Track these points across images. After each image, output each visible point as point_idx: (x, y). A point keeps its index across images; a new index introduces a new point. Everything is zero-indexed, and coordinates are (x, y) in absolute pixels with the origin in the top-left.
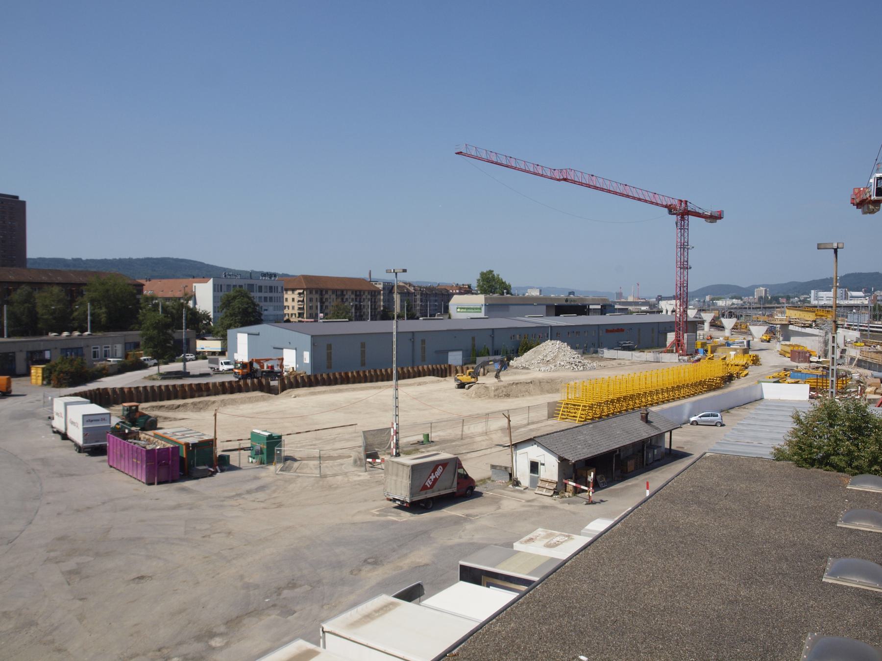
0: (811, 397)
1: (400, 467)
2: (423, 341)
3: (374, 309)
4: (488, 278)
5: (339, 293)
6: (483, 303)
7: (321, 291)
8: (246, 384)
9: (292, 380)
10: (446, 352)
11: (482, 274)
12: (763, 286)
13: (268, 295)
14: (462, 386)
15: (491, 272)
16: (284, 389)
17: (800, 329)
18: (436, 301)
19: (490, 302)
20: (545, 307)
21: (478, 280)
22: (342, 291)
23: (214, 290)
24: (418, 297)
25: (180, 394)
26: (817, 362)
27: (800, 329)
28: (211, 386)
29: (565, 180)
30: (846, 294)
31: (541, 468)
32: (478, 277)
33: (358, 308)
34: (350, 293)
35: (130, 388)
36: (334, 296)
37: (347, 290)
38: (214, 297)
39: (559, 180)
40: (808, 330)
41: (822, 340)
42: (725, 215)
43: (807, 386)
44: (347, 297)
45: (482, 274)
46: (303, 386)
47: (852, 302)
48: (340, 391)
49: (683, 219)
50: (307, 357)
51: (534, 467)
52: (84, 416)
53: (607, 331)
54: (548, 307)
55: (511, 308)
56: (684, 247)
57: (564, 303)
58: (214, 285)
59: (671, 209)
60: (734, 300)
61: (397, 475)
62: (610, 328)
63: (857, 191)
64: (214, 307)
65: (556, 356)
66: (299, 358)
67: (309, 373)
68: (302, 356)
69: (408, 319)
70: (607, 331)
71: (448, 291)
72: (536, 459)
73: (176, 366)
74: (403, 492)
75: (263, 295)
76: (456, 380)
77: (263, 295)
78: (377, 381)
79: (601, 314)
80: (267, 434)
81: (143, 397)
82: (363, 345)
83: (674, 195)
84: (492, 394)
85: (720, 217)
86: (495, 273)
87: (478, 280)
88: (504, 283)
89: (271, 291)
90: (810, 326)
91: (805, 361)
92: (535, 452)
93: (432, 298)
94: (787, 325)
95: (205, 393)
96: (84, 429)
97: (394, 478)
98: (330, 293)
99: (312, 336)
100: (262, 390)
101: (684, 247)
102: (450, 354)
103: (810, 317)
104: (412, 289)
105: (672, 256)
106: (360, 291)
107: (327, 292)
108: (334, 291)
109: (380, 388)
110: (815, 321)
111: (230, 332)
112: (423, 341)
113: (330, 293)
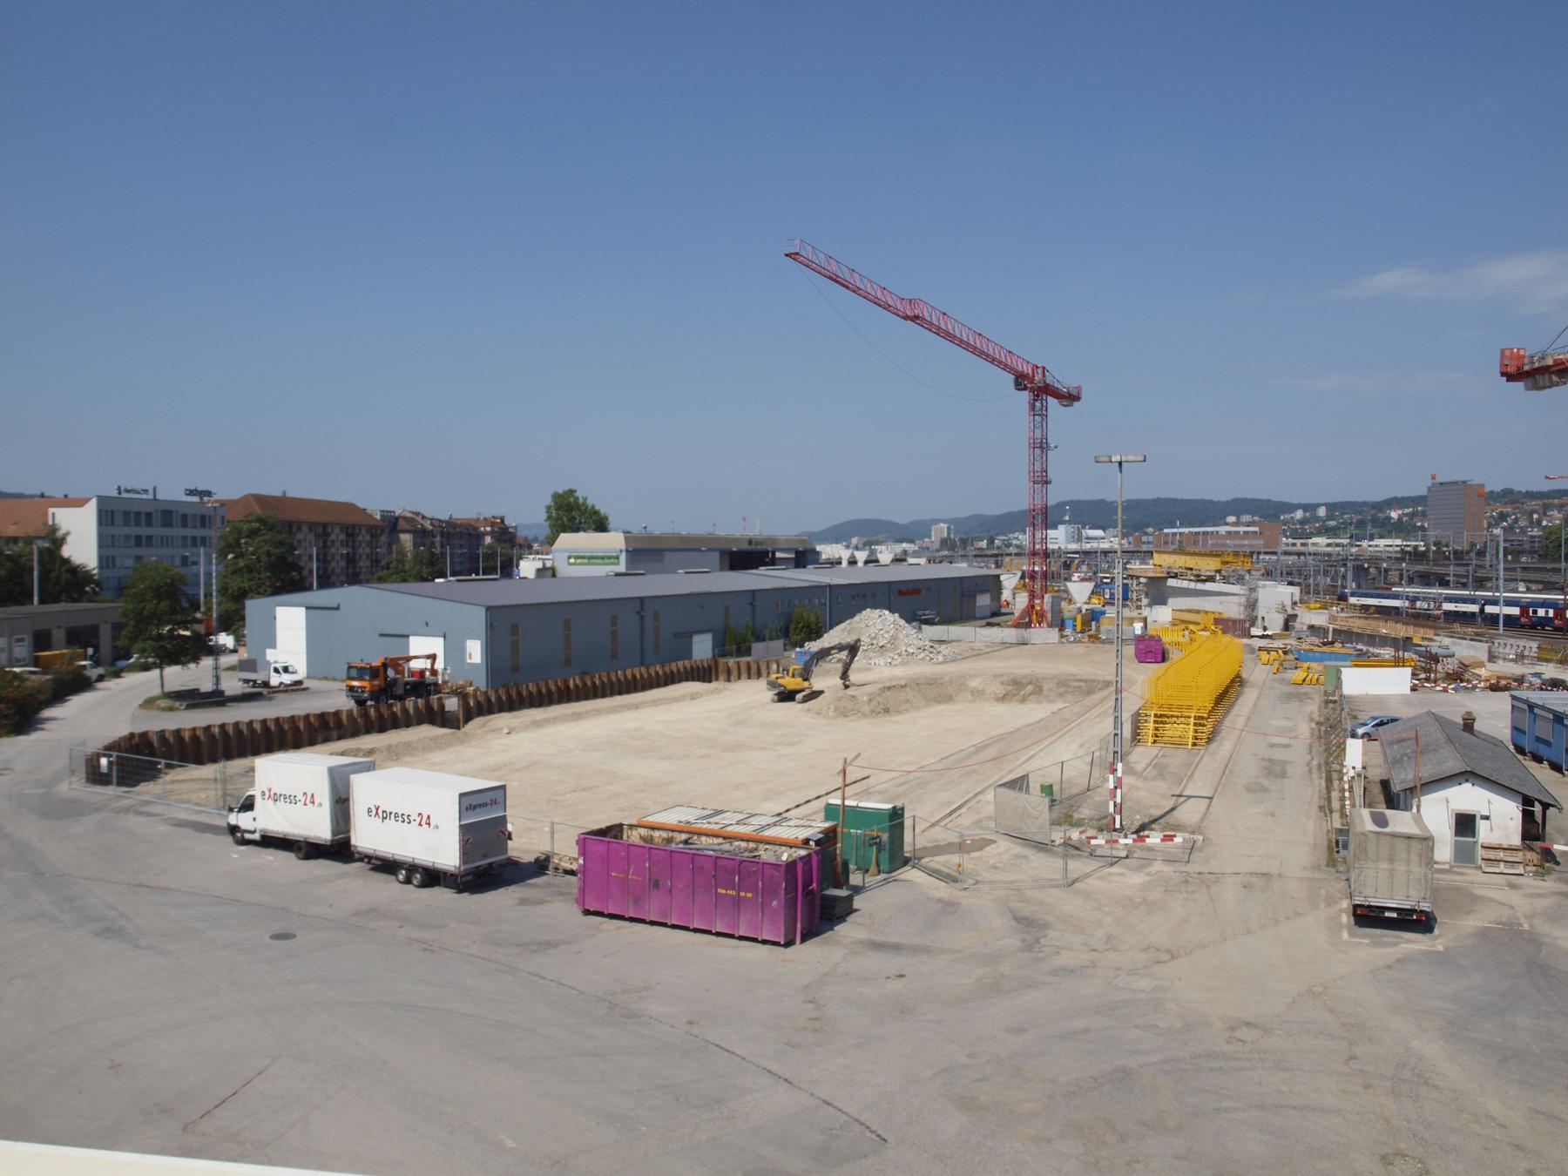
0: (1414, 689)
1: (1401, 845)
2: (656, 616)
3: (324, 560)
4: (568, 504)
5: (320, 530)
6: (623, 546)
7: (290, 526)
9: (481, 699)
10: (689, 635)
11: (556, 497)
12: (944, 521)
14: (786, 696)
15: (572, 492)
17: (1192, 585)
18: (461, 546)
21: (548, 508)
22: (325, 526)
23: (101, 522)
24: (438, 539)
25: (289, 736)
26: (1263, 637)
27: (1192, 585)
28: (344, 717)
29: (915, 318)
30: (1080, 534)
31: (1482, 826)
32: (549, 501)
33: (351, 560)
35: (194, 729)
36: (311, 537)
37: (333, 525)
39: (906, 318)
40: (1209, 586)
41: (1243, 600)
42: (1083, 395)
43: (1409, 671)
44: (333, 537)
45: (556, 497)
46: (501, 710)
47: (1087, 547)
48: (578, 717)
49: (1037, 397)
50: (475, 651)
51: (1465, 824)
53: (901, 593)
54: (723, 553)
55: (668, 555)
57: (746, 547)
59: (1021, 381)
60: (905, 545)
61: (1391, 860)
63: (1507, 353)
64: (101, 558)
65: (894, 638)
70: (901, 593)
71: (476, 529)
72: (1467, 807)
73: (197, 676)
74: (1412, 893)
75: (189, 532)
76: (773, 685)
78: (612, 694)
79: (797, 566)
80: (890, 806)
81: (220, 748)
82: (568, 625)
83: (1031, 352)
86: (580, 494)
87: (548, 508)
88: (596, 513)
89: (203, 525)
90: (1211, 579)
93: (457, 542)
95: (335, 733)
97: (1385, 865)
98: (305, 529)
99: (489, 609)
100: (432, 722)
103: (1208, 565)
106: (354, 526)
107: (299, 529)
108: (312, 526)
109: (637, 707)
110: (1219, 571)
112: (656, 616)
113: (305, 529)
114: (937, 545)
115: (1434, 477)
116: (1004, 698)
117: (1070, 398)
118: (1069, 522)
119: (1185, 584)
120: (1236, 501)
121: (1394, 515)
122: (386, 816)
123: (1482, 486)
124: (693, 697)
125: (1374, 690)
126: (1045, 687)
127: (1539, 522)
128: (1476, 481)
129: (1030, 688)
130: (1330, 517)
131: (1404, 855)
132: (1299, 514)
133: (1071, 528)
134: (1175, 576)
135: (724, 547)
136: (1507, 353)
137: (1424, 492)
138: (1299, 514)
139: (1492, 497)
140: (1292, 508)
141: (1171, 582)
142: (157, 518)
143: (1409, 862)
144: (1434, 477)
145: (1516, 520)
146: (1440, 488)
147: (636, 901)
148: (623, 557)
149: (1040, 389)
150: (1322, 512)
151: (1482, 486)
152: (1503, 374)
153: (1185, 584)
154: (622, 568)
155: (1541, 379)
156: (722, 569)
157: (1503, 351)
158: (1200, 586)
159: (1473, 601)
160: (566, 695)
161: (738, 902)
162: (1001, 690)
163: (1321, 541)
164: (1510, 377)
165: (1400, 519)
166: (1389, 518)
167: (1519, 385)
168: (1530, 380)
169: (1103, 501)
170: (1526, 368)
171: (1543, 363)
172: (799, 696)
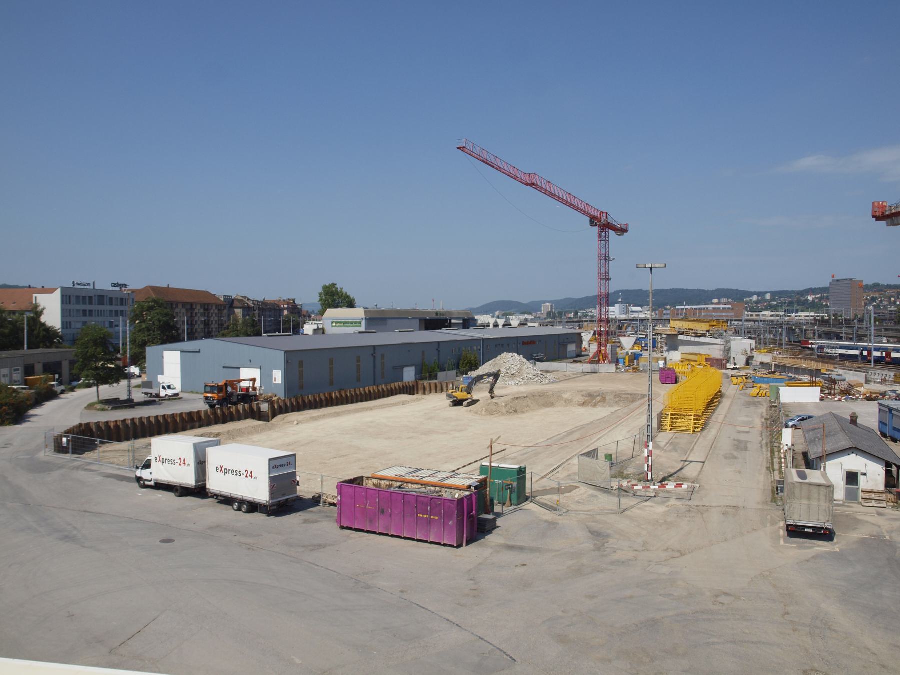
1: (815, 490)
4: (332, 292)
5: (189, 307)
6: (364, 317)
8: (238, 411)
11: (325, 288)
12: (549, 302)
13: (120, 308)
14: (458, 403)
15: (334, 285)
16: (274, 415)
17: (693, 339)
20: (418, 321)
21: (321, 294)
22: (192, 304)
23: (63, 302)
24: (257, 312)
25: (180, 426)
26: (734, 369)
27: (693, 339)
30: (627, 309)
31: (862, 479)
32: (321, 290)
33: (207, 324)
35: (116, 422)
37: (196, 304)
38: (63, 310)
39: (527, 184)
40: (703, 340)
41: (723, 347)
42: (630, 229)
43: (819, 389)
44: (197, 311)
48: (338, 415)
49: (603, 230)
50: (278, 377)
51: (852, 478)
52: (270, 460)
53: (524, 344)
57: (434, 317)
58: (63, 296)
60: (526, 316)
61: (809, 499)
62: (526, 341)
64: (63, 323)
65: (520, 369)
66: (266, 377)
68: (271, 376)
70: (524, 344)
71: (279, 306)
72: (853, 468)
74: (821, 518)
75: (114, 308)
76: (450, 396)
77: (114, 308)
79: (464, 328)
82: (331, 362)
83: (599, 204)
84: (504, 410)
85: (627, 231)
87: (321, 294)
88: (348, 297)
89: (122, 304)
90: (704, 336)
91: (723, 369)
93: (268, 313)
94: (677, 335)
95: (197, 424)
96: (272, 479)
97: (805, 502)
98: (180, 306)
99: (286, 352)
102: (405, 369)
103: (702, 328)
104: (251, 304)
105: (594, 265)
106: (208, 305)
107: (177, 306)
108: (184, 305)
110: (708, 331)
113: (180, 306)
115: (833, 277)
116: (583, 404)
117: (622, 231)
118: (621, 303)
119: (689, 338)
120: (718, 290)
121: (810, 298)
122: (227, 472)
124: (404, 403)
125: (798, 400)
128: (858, 279)
129: (599, 399)
130: (773, 300)
131: (816, 495)
132: (755, 298)
133: (623, 306)
136: (876, 205)
137: (828, 285)
138: (755, 298)
139: (867, 288)
140: (751, 294)
141: (681, 337)
142: (95, 300)
143: (819, 500)
144: (833, 277)
145: (881, 302)
147: (371, 521)
148: (363, 323)
149: (604, 226)
150: (768, 297)
152: (874, 217)
153: (689, 338)
154: (363, 329)
156: (420, 330)
157: (873, 204)
158: (697, 340)
159: (856, 349)
160: (330, 402)
161: (430, 522)
162: (582, 400)
163: (768, 313)
164: (878, 219)
165: (814, 301)
166: (808, 300)
167: (883, 223)
168: (889, 220)
170: (887, 213)
172: (465, 403)
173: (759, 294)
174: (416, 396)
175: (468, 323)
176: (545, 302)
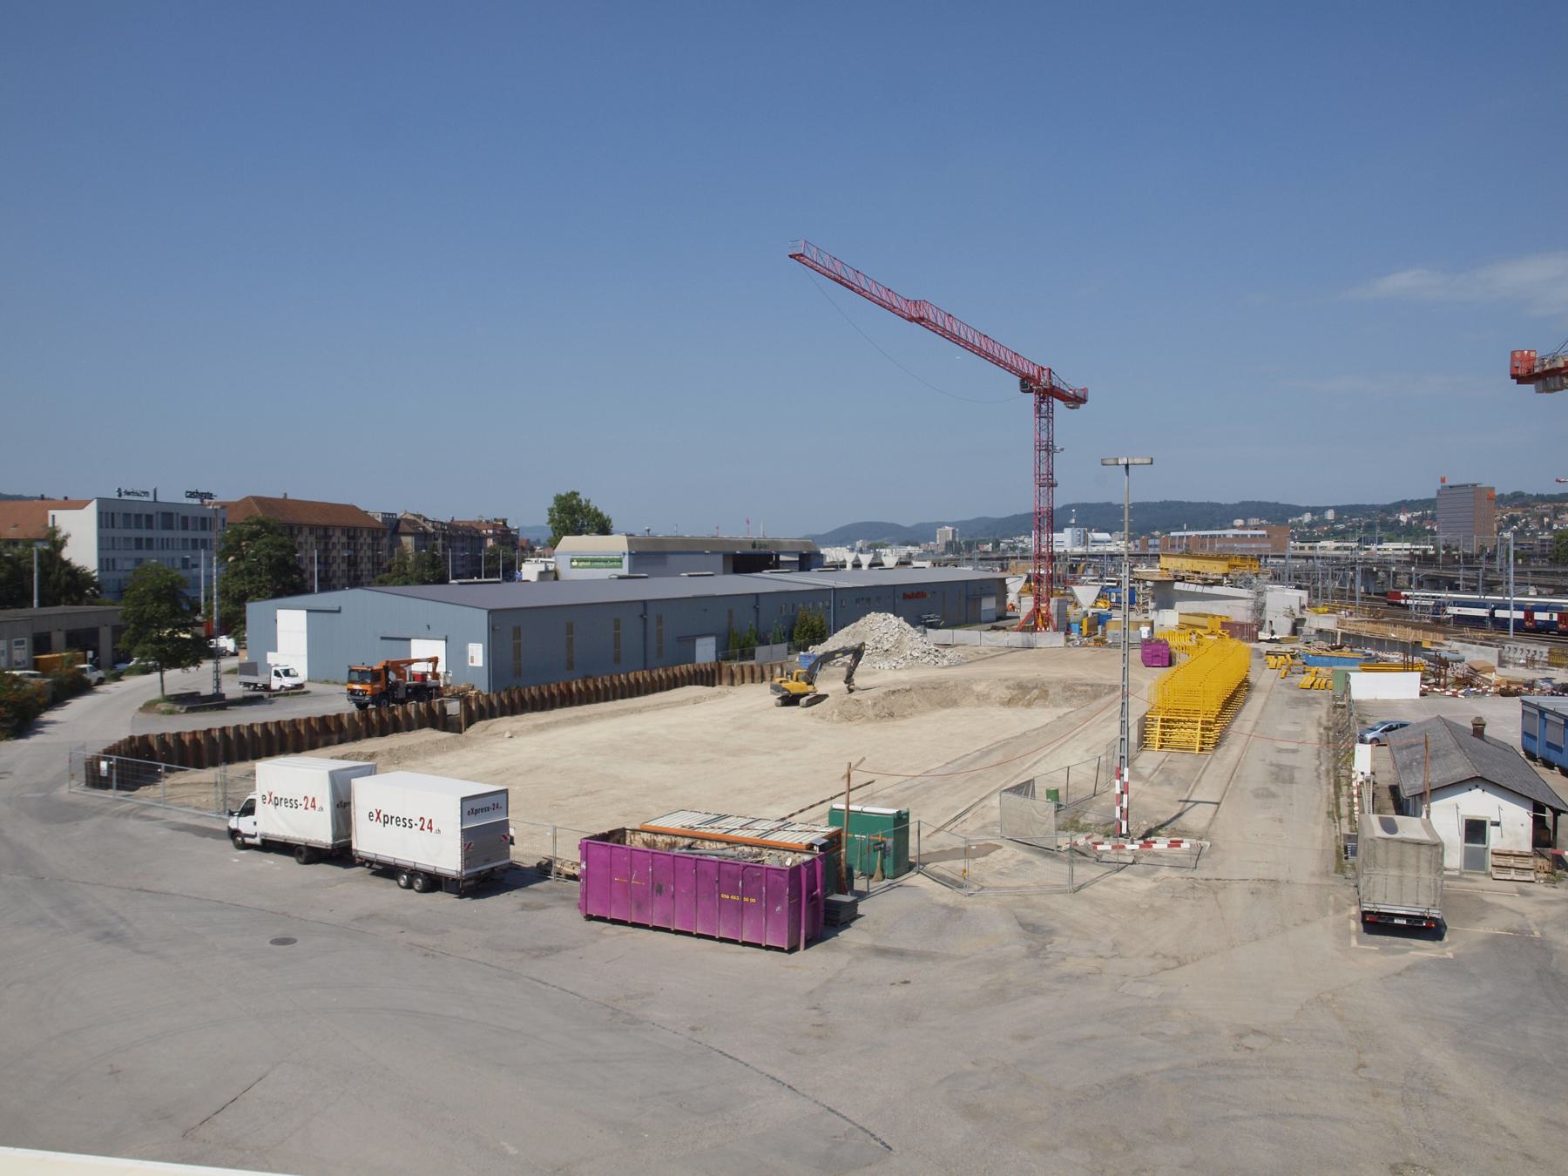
0: (1423, 694)
1: (1410, 851)
2: (660, 620)
3: (325, 562)
4: (571, 507)
5: (321, 532)
8: (406, 714)
9: (483, 702)
11: (559, 499)
14: (790, 700)
15: (575, 494)
17: (1199, 589)
18: (463, 549)
19: (643, 549)
21: (551, 510)
22: (326, 528)
23: (100, 525)
24: (440, 541)
25: (306, 740)
26: (1271, 641)
27: (1199, 589)
28: (345, 721)
30: (1086, 537)
31: (1492, 832)
32: (551, 504)
34: (338, 533)
36: (312, 539)
39: (911, 319)
40: (1216, 590)
41: (1251, 603)
42: (1090, 398)
43: (1418, 675)
44: (334, 540)
45: (559, 499)
49: (1042, 400)
50: (477, 654)
51: (1475, 830)
52: (463, 800)
53: (906, 597)
54: (726, 556)
55: (671, 558)
56: (1047, 448)
57: (750, 550)
58: (100, 514)
61: (1401, 866)
64: (101, 561)
65: (899, 641)
66: (457, 655)
67: (485, 690)
69: (321, 590)
70: (906, 597)
71: (478, 531)
73: (197, 679)
74: (1422, 899)
76: (776, 689)
82: (570, 629)
83: (1036, 355)
84: (871, 713)
85: (1084, 401)
87: (551, 510)
88: (599, 515)
89: (204, 528)
90: (1218, 583)
92: (1479, 803)
93: (459, 544)
97: (1393, 872)
98: (306, 531)
99: (490, 612)
101: (1047, 448)
102: (699, 642)
103: (1215, 569)
106: (355, 529)
107: (300, 531)
108: (313, 529)
110: (1226, 575)
111: (254, 609)
112: (660, 620)
113: (306, 531)
114: (942, 549)
115: (1443, 480)
116: (1009, 702)
117: (1076, 400)
118: (1075, 525)
119: (1192, 588)
120: (1243, 504)
121: (1403, 518)
122: (387, 820)
123: (1492, 489)
125: (1383, 695)
126: (1051, 692)
127: (1550, 525)
128: (1485, 485)
129: (1036, 692)
130: (1338, 520)
131: (1413, 861)
132: (1307, 518)
133: (1078, 531)
134: (1182, 580)
135: (728, 549)
136: (1518, 355)
137: (1433, 495)
138: (1307, 518)
139: (1502, 500)
140: (1300, 511)
141: (1178, 586)
143: (1418, 868)
144: (1443, 480)
145: (1526, 524)
146: (1451, 491)
147: (639, 906)
148: (626, 560)
149: (1045, 392)
150: (1330, 515)
151: (1492, 489)
152: (1513, 377)
153: (1192, 588)
154: (625, 571)
155: (1552, 382)
156: (725, 573)
157: (1513, 353)
158: (1207, 590)
161: (741, 908)
162: (1007, 694)
163: (1330, 544)
164: (1521, 379)
165: (1409, 522)
168: (1540, 383)
169: (1109, 504)
170: (1537, 370)
171: (1554, 365)
172: (803, 700)
173: (1314, 511)
174: (717, 688)
175: (808, 560)
176: (942, 525)
